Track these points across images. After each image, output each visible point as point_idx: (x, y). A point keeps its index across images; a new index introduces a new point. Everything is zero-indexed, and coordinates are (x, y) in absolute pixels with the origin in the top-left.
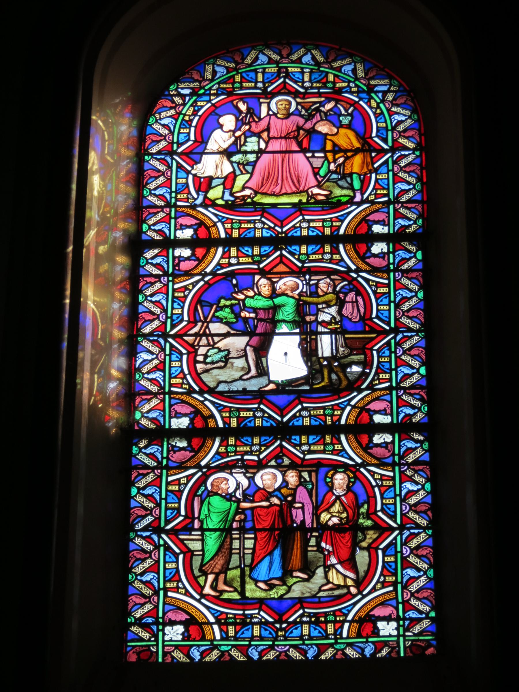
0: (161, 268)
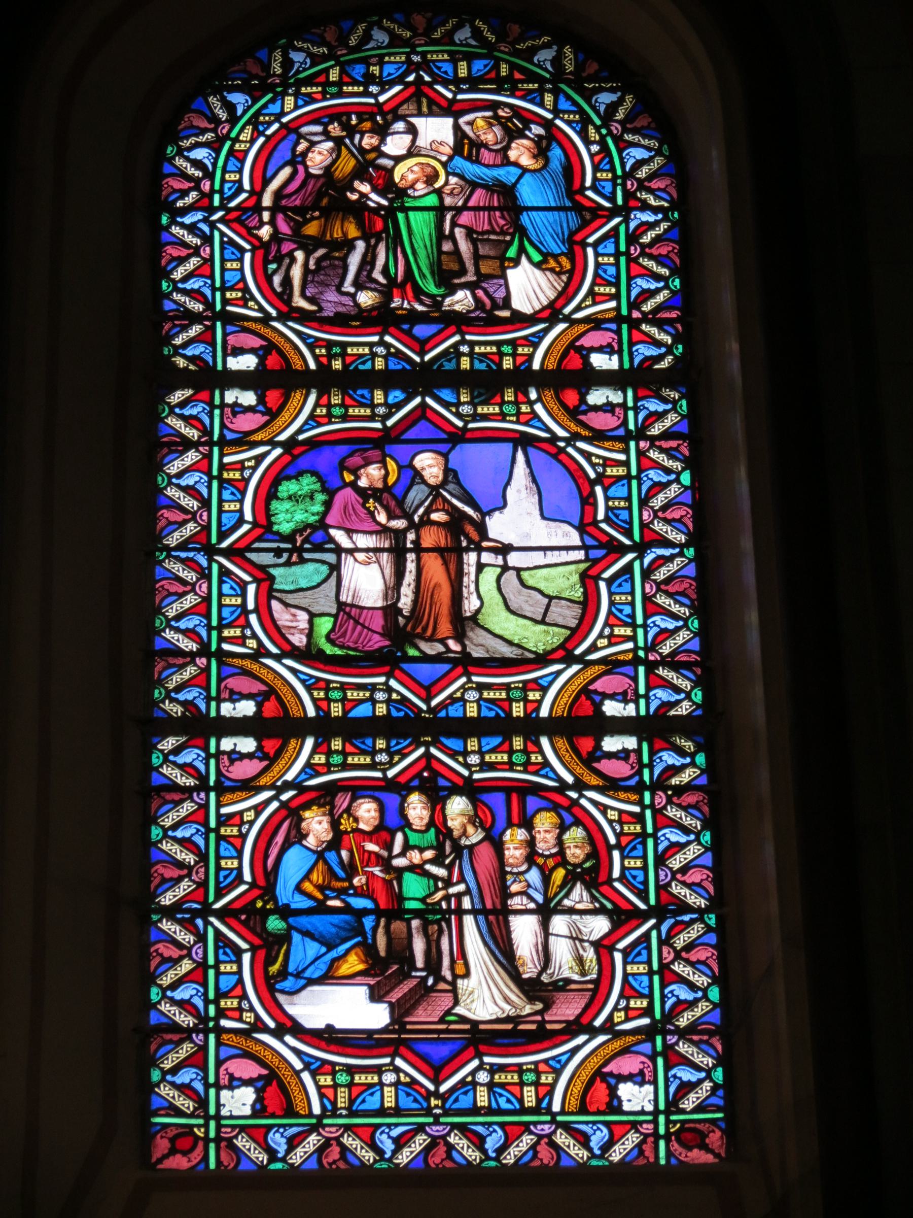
0: (196, 638)
